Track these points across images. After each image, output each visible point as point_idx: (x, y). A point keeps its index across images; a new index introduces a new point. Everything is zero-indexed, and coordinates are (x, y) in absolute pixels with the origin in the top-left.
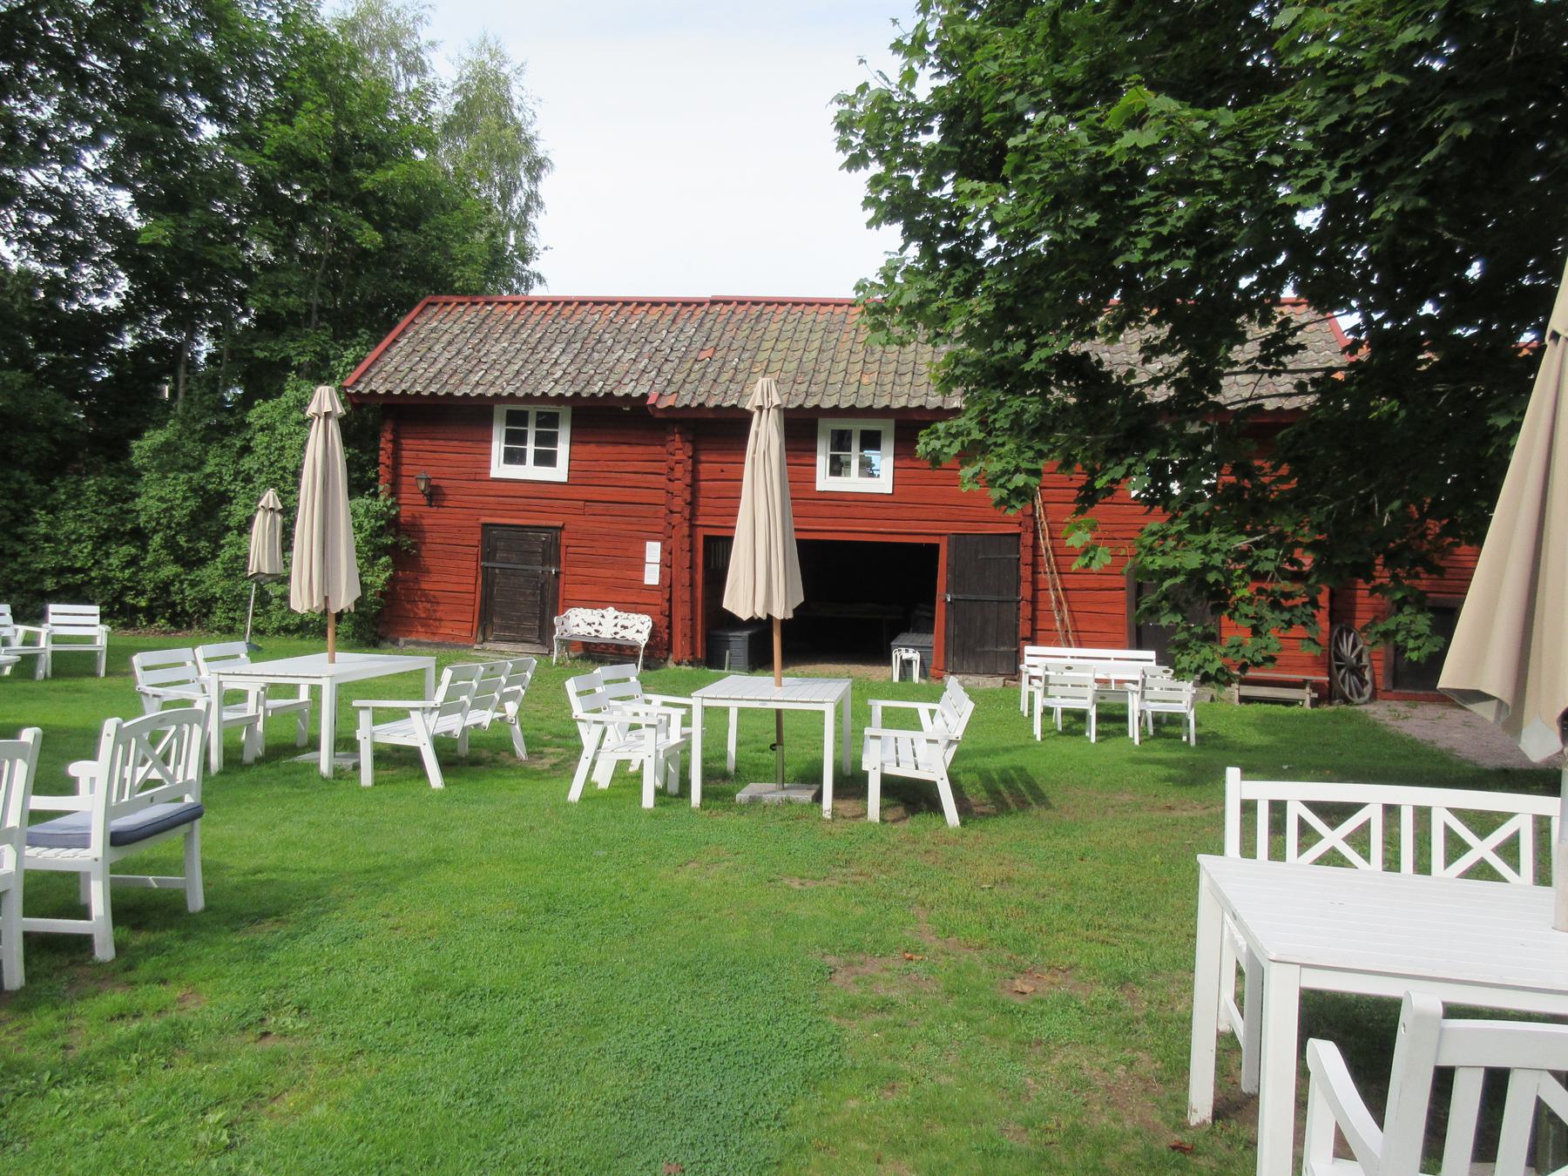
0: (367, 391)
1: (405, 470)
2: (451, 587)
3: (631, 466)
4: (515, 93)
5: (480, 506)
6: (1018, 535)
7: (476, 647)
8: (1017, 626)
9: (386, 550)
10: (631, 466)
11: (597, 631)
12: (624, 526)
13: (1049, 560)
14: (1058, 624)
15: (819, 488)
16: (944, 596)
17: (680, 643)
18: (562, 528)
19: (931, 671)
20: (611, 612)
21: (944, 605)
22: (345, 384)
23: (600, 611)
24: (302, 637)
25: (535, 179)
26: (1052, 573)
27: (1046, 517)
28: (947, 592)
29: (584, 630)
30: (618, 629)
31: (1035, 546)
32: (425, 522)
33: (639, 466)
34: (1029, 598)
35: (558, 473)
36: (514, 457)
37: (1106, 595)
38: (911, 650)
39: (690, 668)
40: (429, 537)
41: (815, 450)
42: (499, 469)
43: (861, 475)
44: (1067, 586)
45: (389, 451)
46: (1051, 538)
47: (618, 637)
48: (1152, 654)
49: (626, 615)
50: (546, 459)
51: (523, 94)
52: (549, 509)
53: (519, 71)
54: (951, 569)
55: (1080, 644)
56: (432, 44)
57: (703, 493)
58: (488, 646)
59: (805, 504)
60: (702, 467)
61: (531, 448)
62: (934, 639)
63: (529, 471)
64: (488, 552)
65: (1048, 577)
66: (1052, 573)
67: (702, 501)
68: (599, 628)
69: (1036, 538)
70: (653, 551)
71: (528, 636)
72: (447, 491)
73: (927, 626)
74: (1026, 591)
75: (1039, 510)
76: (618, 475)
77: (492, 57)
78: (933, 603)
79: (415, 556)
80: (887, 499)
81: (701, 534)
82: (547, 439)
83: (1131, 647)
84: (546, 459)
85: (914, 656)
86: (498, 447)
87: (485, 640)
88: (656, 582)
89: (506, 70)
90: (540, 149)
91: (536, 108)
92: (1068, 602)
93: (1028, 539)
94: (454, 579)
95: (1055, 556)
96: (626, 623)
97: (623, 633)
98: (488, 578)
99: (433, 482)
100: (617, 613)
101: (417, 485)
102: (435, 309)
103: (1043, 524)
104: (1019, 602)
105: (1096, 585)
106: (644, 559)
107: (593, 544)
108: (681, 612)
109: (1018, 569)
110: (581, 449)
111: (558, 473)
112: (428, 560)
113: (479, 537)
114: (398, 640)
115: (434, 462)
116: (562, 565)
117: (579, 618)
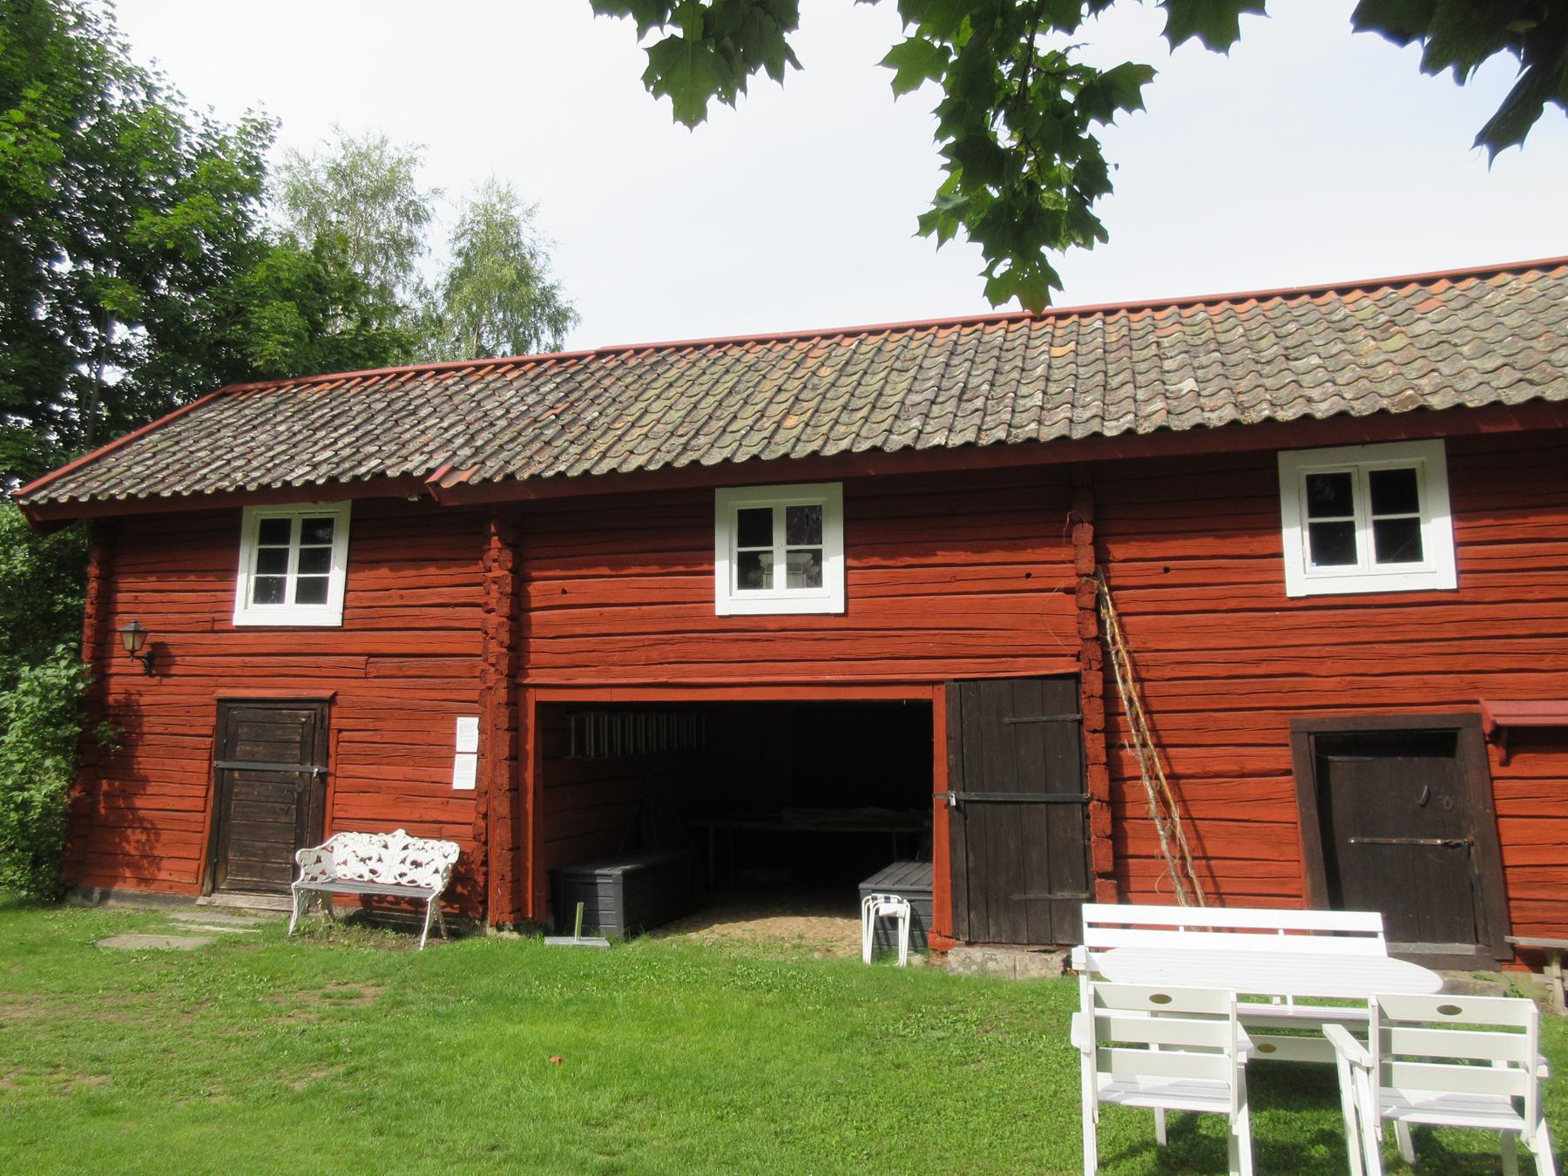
3: (433, 596)
4: (526, 238)
5: (219, 670)
6: (1076, 677)
7: (201, 900)
8: (1086, 849)
10: (433, 596)
11: (373, 872)
13: (1136, 719)
14: (1164, 845)
16: (946, 797)
17: (499, 895)
18: (332, 701)
19: (930, 937)
21: (946, 812)
23: (382, 837)
25: (557, 332)
26: (1144, 745)
27: (1126, 642)
28: (950, 788)
29: (353, 870)
30: (406, 868)
31: (1109, 696)
33: (447, 594)
34: (1105, 795)
35: (328, 613)
36: (268, 592)
37: (1252, 786)
38: (894, 898)
39: (515, 936)
40: (151, 723)
41: (711, 548)
42: (247, 611)
43: (790, 584)
44: (1179, 770)
46: (1138, 679)
47: (404, 881)
48: (1373, 920)
49: (420, 843)
50: (312, 592)
51: (536, 237)
52: (317, 672)
53: (530, 213)
54: (957, 744)
55: (1219, 898)
56: (435, 191)
57: (535, 630)
58: (219, 899)
59: (699, 641)
60: (535, 588)
61: (292, 578)
62: (931, 875)
63: (289, 612)
64: (224, 743)
65: (1137, 754)
66: (1144, 745)
67: (534, 644)
69: (1109, 681)
70: (467, 732)
72: (173, 651)
73: (916, 848)
74: (1098, 782)
75: (1112, 629)
76: (416, 611)
77: (501, 200)
78: (928, 803)
80: (834, 623)
81: (533, 697)
82: (316, 561)
83: (1316, 905)
84: (312, 592)
85: (899, 908)
86: (245, 581)
87: (214, 889)
89: (516, 212)
90: (562, 299)
91: (550, 251)
92: (1182, 800)
93: (1094, 683)
95: (1148, 712)
96: (421, 857)
97: (414, 874)
98: (222, 785)
100: (409, 840)
103: (1120, 653)
104: (1085, 804)
105: (1234, 768)
106: (454, 745)
107: (378, 725)
108: (501, 835)
109: (1080, 740)
111: (328, 613)
112: (146, 763)
113: (212, 720)
115: (158, 607)
116: (332, 761)
117: (349, 849)
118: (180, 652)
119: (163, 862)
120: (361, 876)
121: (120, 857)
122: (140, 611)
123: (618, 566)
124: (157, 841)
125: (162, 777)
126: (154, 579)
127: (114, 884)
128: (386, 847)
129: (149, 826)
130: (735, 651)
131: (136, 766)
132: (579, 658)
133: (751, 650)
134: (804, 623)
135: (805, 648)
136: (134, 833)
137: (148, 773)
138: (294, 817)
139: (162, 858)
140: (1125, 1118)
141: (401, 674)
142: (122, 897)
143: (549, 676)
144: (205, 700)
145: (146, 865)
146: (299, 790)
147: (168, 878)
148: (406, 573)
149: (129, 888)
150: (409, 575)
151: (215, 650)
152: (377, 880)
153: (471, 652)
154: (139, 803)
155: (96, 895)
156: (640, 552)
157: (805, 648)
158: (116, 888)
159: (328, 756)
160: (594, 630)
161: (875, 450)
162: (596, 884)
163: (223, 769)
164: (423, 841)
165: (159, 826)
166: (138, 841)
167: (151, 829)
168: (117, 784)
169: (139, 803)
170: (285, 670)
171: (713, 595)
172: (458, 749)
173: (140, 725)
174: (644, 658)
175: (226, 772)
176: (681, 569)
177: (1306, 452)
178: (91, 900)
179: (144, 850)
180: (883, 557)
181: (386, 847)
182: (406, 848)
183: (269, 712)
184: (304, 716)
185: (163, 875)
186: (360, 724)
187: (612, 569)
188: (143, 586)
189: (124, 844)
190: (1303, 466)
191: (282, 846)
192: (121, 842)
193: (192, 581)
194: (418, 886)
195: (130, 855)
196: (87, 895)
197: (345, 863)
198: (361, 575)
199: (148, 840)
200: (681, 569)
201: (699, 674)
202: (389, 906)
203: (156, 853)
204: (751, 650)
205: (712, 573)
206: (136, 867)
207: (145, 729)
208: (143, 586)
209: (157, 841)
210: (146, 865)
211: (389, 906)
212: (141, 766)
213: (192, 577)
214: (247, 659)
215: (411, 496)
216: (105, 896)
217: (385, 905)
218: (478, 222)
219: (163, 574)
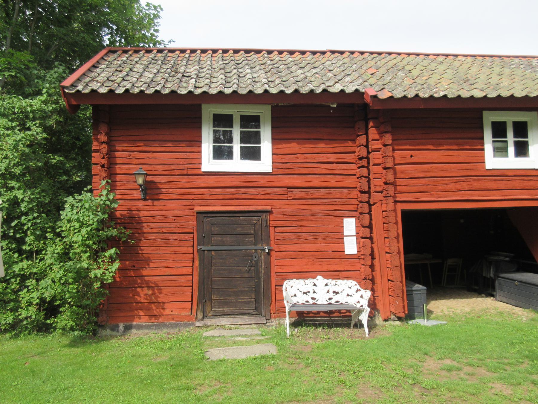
0: (87, 91)
1: (119, 168)
2: (168, 271)
7: (198, 324)
9: (111, 242)
11: (313, 299)
12: (323, 207)
15: (487, 167)
20: (320, 280)
22: (64, 84)
23: (310, 281)
24: (17, 336)
29: (301, 299)
30: (331, 295)
32: (142, 214)
40: (146, 227)
45: (104, 151)
47: (333, 301)
49: (334, 282)
59: (478, 180)
61: (237, 147)
68: (314, 296)
71: (245, 310)
72: (160, 186)
79: (133, 246)
88: (355, 252)
94: (171, 263)
97: (336, 298)
99: (149, 179)
100: (326, 281)
101: (135, 181)
102: (115, 55)
107: (298, 223)
110: (285, 147)
113: (195, 224)
114: (118, 326)
116: (272, 242)
118: (165, 186)
119: (165, 305)
120: (307, 302)
121: (134, 304)
122: (134, 162)
123: (437, 146)
124: (160, 293)
125: (160, 257)
126: (142, 144)
127: (133, 321)
128: (315, 285)
129: (153, 285)
130: (494, 185)
131: (140, 252)
132: (422, 188)
133: (502, 185)
134: (523, 173)
135: (526, 184)
136: (142, 290)
137: (149, 255)
138: (254, 274)
139: (164, 303)
140: (357, 389)
141: (309, 197)
142: (140, 327)
143: (407, 197)
144: (187, 212)
145: (154, 308)
146: (256, 259)
147: (171, 313)
148: (307, 146)
149: (144, 322)
150: (309, 147)
151: (188, 185)
152: (317, 303)
153: (348, 186)
154: (145, 272)
155: (121, 327)
156: (447, 139)
157: (526, 184)
158: (135, 323)
159: (270, 241)
160: (428, 175)
161: (173, 92)
162: (412, 294)
163: (204, 251)
164: (334, 281)
165: (160, 285)
166: (146, 295)
167: (155, 287)
168: (127, 263)
169: (145, 272)
170: (237, 196)
171: (484, 159)
172: (345, 234)
173: (142, 228)
174: (454, 188)
175: (206, 252)
176: (468, 147)
177: (257, 105)
178: (118, 331)
179: (151, 299)
180: (128, 144)
181: (315, 285)
182: (326, 285)
183: (232, 218)
184: (256, 220)
185: (167, 312)
186: (288, 223)
187: (434, 146)
188: (133, 148)
189: (136, 297)
190: (212, 109)
191: (247, 289)
192: (134, 296)
193: (169, 146)
194: (342, 304)
195: (141, 303)
196: (115, 328)
197: (295, 295)
198: (280, 146)
199: (154, 294)
200: (468, 147)
201: (494, 196)
202: (313, 315)
203: (159, 300)
204: (502, 185)
205: (483, 150)
206: (146, 309)
207: (145, 231)
208: (133, 148)
209: (160, 293)
210: (154, 308)
211: (313, 315)
212: (143, 252)
213: (170, 144)
214: (211, 190)
215: (333, 104)
216: (128, 328)
217: (311, 315)
218: (387, 140)
219: (147, 141)
